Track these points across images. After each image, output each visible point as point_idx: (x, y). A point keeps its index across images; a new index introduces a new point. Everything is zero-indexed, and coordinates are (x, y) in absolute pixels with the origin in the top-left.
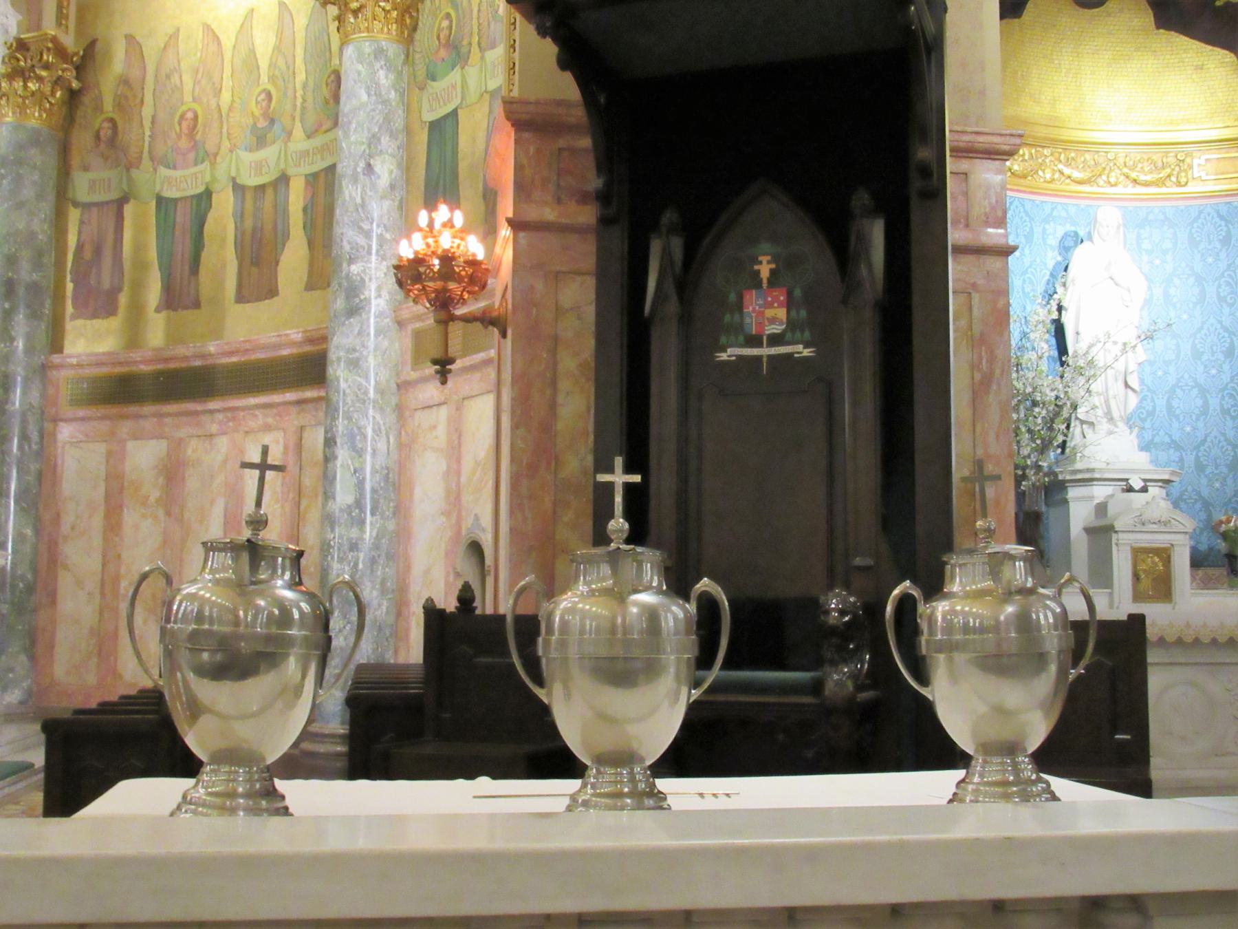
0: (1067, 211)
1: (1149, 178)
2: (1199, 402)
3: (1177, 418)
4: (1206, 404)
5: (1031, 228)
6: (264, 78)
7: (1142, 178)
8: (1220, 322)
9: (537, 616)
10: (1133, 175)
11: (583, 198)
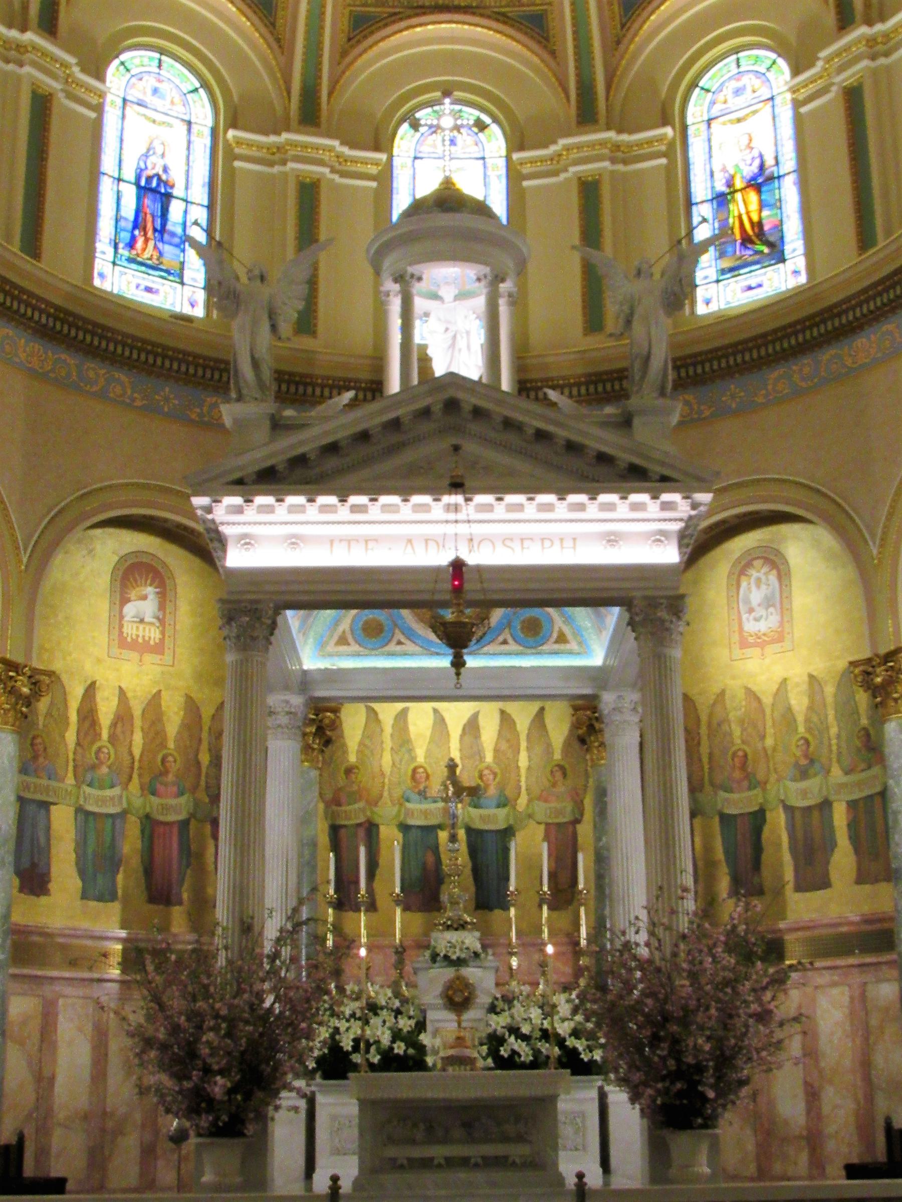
6: (801, 729)
9: (84, 896)
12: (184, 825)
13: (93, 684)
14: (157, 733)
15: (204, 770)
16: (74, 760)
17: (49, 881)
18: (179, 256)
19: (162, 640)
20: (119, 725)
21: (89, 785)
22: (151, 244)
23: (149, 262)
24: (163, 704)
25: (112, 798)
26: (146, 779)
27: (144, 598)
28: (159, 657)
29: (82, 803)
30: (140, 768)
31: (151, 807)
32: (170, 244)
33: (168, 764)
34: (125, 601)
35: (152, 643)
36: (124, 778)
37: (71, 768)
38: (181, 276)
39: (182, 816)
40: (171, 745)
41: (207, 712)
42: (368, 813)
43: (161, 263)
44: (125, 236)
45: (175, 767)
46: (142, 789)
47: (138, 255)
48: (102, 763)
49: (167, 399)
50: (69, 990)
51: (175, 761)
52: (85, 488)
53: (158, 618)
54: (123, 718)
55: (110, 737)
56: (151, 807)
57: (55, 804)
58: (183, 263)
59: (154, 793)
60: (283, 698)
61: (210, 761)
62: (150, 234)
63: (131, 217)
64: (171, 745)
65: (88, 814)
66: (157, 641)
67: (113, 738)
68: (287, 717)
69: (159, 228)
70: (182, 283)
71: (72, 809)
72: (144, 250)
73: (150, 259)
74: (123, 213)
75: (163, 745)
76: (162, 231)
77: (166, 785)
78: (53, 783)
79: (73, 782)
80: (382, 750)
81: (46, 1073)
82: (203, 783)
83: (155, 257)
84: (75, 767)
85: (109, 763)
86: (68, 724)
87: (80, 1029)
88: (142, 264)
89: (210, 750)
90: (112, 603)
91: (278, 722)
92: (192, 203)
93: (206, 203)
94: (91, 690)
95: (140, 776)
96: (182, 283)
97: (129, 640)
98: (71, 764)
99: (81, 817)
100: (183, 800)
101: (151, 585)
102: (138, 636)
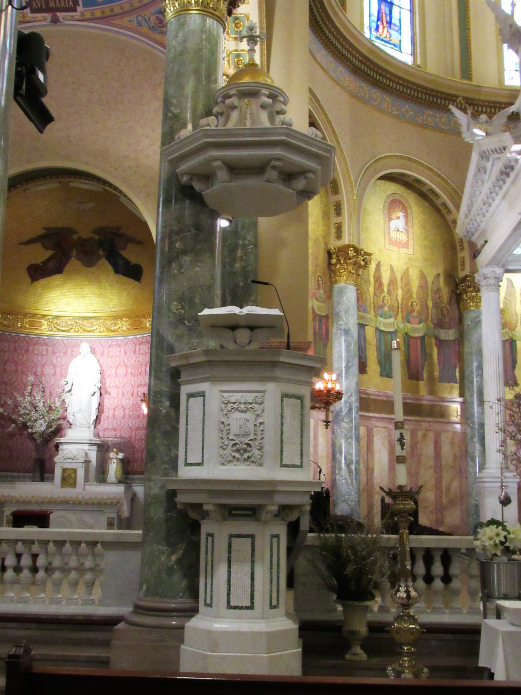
0: (117, 342)
1: (63, 329)
2: (123, 413)
3: (116, 418)
4: (125, 414)
5: (103, 351)
7: (61, 329)
8: (131, 382)
10: (58, 327)
11: (411, 488)
12: (423, 338)
13: (379, 263)
14: (408, 290)
15: (430, 310)
16: (374, 303)
17: (367, 366)
18: (398, 37)
19: (408, 241)
20: (391, 285)
21: (380, 316)
22: (386, 29)
23: (385, 39)
24: (410, 274)
25: (390, 324)
26: (405, 314)
27: (398, 218)
28: (407, 250)
29: (378, 325)
30: (401, 308)
31: (408, 329)
32: (394, 30)
33: (414, 307)
34: (390, 219)
35: (403, 242)
36: (395, 313)
37: (372, 307)
38: (400, 48)
39: (421, 334)
40: (414, 296)
41: (430, 279)
42: (510, 335)
43: (391, 40)
44: (374, 25)
45: (417, 308)
46: (403, 319)
47: (380, 35)
48: (385, 305)
49: (407, 111)
50: (378, 424)
51: (417, 305)
52: (375, 157)
53: (405, 229)
54: (392, 282)
55: (388, 291)
56: (408, 329)
57: (367, 326)
58: (400, 41)
59: (409, 322)
60: (492, 269)
61: (433, 306)
62: (385, 24)
63: (376, 15)
64: (414, 296)
65: (381, 331)
66: (406, 241)
67: (389, 292)
68: (494, 280)
69: (388, 21)
70: (401, 52)
71: (374, 329)
72: (383, 32)
73: (386, 38)
74: (372, 12)
75: (411, 296)
76: (390, 23)
77: (412, 317)
78: (365, 314)
79: (374, 314)
80: (516, 302)
81: (371, 466)
82: (430, 318)
83: (388, 37)
84: (374, 306)
85: (388, 305)
86: (370, 283)
87: (383, 444)
88: (382, 40)
89: (432, 300)
90: (385, 221)
91: (490, 283)
92: (403, 8)
93: (409, 9)
94: (378, 265)
95: (402, 312)
96: (401, 52)
97: (393, 240)
98: (372, 305)
99: (378, 333)
100: (421, 326)
101: (401, 211)
102: (397, 238)
